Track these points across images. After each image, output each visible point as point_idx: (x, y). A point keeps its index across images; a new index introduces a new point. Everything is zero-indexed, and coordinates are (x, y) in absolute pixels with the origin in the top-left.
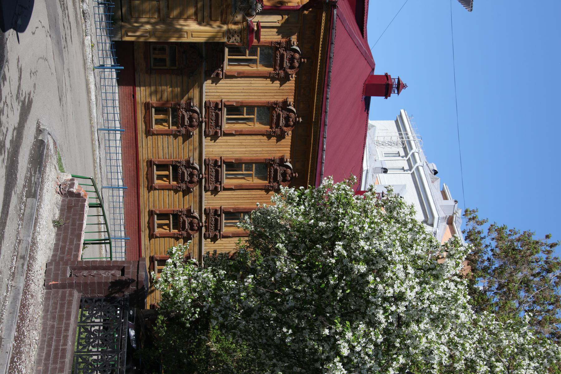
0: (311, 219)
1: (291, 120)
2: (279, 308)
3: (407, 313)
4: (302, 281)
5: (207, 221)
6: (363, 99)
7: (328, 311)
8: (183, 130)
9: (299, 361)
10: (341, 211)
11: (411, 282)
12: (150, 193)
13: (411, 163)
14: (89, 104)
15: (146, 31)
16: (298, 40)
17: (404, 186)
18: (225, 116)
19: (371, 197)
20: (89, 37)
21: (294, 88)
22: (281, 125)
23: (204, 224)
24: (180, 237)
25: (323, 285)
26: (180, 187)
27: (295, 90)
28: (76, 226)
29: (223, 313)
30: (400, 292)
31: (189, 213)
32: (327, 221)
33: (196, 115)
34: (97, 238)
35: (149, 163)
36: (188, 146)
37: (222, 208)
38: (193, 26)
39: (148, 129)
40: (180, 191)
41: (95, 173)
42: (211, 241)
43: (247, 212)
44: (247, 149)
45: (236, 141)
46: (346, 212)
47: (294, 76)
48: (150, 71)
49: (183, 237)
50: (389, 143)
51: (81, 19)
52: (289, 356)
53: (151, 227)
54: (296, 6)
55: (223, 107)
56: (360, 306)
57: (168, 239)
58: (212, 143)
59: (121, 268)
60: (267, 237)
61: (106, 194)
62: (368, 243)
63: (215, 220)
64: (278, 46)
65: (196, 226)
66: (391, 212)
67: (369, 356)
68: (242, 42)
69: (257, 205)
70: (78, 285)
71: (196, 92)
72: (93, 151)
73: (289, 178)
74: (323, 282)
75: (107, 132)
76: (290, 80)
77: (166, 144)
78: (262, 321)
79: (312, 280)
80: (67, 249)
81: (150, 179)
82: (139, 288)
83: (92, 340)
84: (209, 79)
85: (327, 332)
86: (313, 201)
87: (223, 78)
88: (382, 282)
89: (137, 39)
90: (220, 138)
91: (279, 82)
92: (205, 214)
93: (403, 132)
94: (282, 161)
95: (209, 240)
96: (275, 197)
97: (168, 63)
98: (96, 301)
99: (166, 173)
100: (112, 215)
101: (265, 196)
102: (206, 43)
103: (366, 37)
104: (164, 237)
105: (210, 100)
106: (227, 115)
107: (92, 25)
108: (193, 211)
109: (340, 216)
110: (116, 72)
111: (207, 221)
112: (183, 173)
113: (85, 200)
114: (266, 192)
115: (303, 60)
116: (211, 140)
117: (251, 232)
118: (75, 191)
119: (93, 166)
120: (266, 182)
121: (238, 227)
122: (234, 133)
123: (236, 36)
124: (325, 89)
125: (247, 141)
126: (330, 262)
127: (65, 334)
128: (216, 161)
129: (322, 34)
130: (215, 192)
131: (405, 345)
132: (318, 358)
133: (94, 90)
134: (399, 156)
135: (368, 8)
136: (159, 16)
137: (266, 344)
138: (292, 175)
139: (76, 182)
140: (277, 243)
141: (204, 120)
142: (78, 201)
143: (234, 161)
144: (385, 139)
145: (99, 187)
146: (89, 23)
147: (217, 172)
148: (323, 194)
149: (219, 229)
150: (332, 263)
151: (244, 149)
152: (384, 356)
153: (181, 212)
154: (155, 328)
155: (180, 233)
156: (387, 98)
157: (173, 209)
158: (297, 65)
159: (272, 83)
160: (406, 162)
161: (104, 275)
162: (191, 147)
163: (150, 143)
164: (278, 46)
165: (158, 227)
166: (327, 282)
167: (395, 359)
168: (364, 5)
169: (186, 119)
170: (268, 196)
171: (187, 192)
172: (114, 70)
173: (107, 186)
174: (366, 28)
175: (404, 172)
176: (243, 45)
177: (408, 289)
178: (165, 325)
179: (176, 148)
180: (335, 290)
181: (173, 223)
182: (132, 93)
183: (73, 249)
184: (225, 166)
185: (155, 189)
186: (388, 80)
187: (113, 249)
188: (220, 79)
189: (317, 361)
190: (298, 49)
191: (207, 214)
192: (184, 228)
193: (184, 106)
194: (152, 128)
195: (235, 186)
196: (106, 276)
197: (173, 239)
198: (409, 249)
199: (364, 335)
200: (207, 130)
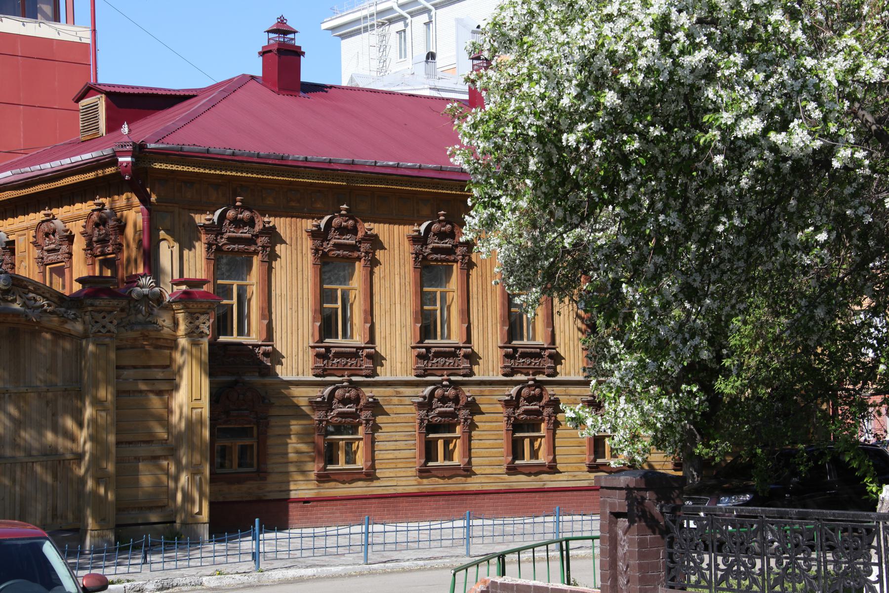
0: (526, 184)
1: (344, 224)
4: (635, 200)
6: (306, 95)
7: (687, 151)
9: (777, 202)
10: (509, 130)
11: (635, 7)
12: (477, 472)
13: (418, 10)
15: (192, 480)
16: (202, 212)
17: (459, 21)
18: (340, 341)
19: (485, 78)
20: (204, 579)
21: (288, 219)
23: (531, 377)
24: (553, 418)
25: (642, 160)
26: (466, 420)
27: (292, 217)
29: (687, 335)
30: (652, 26)
31: (512, 403)
32: (528, 154)
33: (338, 393)
34: (559, 564)
35: (424, 474)
36: (392, 407)
37: (502, 345)
38: (181, 399)
39: (363, 476)
40: (472, 420)
41: (442, 568)
42: (561, 364)
43: (509, 300)
44: (398, 301)
45: (383, 321)
46: (512, 121)
48: (261, 474)
49: (554, 413)
50: (382, 50)
52: (769, 220)
53: (536, 470)
54: (143, 215)
56: (679, 93)
57: (556, 440)
58: (387, 363)
59: (613, 518)
60: (552, 264)
61: (479, 549)
63: (523, 358)
65: (534, 390)
66: (511, 41)
67: (767, 77)
68: (209, 311)
69: (497, 283)
71: (296, 391)
72: (404, 571)
73: (448, 226)
74: (636, 160)
75: (370, 547)
76: (274, 225)
77: (391, 445)
78: (705, 267)
83: (742, 569)
84: (274, 369)
85: (719, 159)
86: (492, 181)
87: (272, 346)
88: (634, 57)
89: (206, 497)
90: (377, 349)
91: (279, 245)
92: (512, 376)
93: (362, 25)
94: (418, 240)
95: (559, 367)
96: (481, 253)
97: (247, 442)
98: (673, 562)
99: (440, 443)
100: (517, 538)
102: (211, 375)
103: (196, 90)
104: (554, 447)
106: (337, 337)
107: (183, 574)
109: (518, 132)
110: (266, 532)
112: (441, 414)
114: (472, 268)
115: (238, 204)
116: (382, 365)
117: (543, 292)
119: (430, 572)
121: (535, 317)
122: (368, 325)
123: (197, 323)
124: (290, 163)
125: (383, 302)
126: (601, 149)
128: (420, 356)
129: (191, 169)
130: (473, 358)
131: (750, 12)
132: (773, 166)
133: (297, 570)
134: (404, 31)
135: (142, 88)
136: (166, 458)
137: (746, 261)
138: (442, 221)
141: (346, 378)
143: (419, 325)
145: (467, 560)
147: (438, 355)
148: (480, 164)
149: (538, 350)
150: (604, 145)
153: (509, 417)
154: (718, 459)
156: (304, 53)
157: (504, 432)
158: (246, 214)
159: (280, 257)
160: (415, 19)
162: (395, 400)
163: (388, 473)
164: (214, 247)
165: (537, 458)
166: (636, 154)
167: (776, 30)
168: (139, 95)
169: (345, 409)
170: (479, 265)
171: (474, 408)
172: (261, 536)
173: (465, 547)
174: (178, 91)
175: (434, 22)
176: (214, 309)
177: (648, 11)
178: (712, 443)
179: (397, 427)
180: (650, 139)
181: (528, 432)
182: (301, 504)
184: (427, 341)
185: (469, 463)
186: (270, 51)
187: (575, 535)
189: (778, 169)
191: (513, 372)
192: (538, 413)
194: (362, 469)
195: (463, 323)
198: (576, 7)
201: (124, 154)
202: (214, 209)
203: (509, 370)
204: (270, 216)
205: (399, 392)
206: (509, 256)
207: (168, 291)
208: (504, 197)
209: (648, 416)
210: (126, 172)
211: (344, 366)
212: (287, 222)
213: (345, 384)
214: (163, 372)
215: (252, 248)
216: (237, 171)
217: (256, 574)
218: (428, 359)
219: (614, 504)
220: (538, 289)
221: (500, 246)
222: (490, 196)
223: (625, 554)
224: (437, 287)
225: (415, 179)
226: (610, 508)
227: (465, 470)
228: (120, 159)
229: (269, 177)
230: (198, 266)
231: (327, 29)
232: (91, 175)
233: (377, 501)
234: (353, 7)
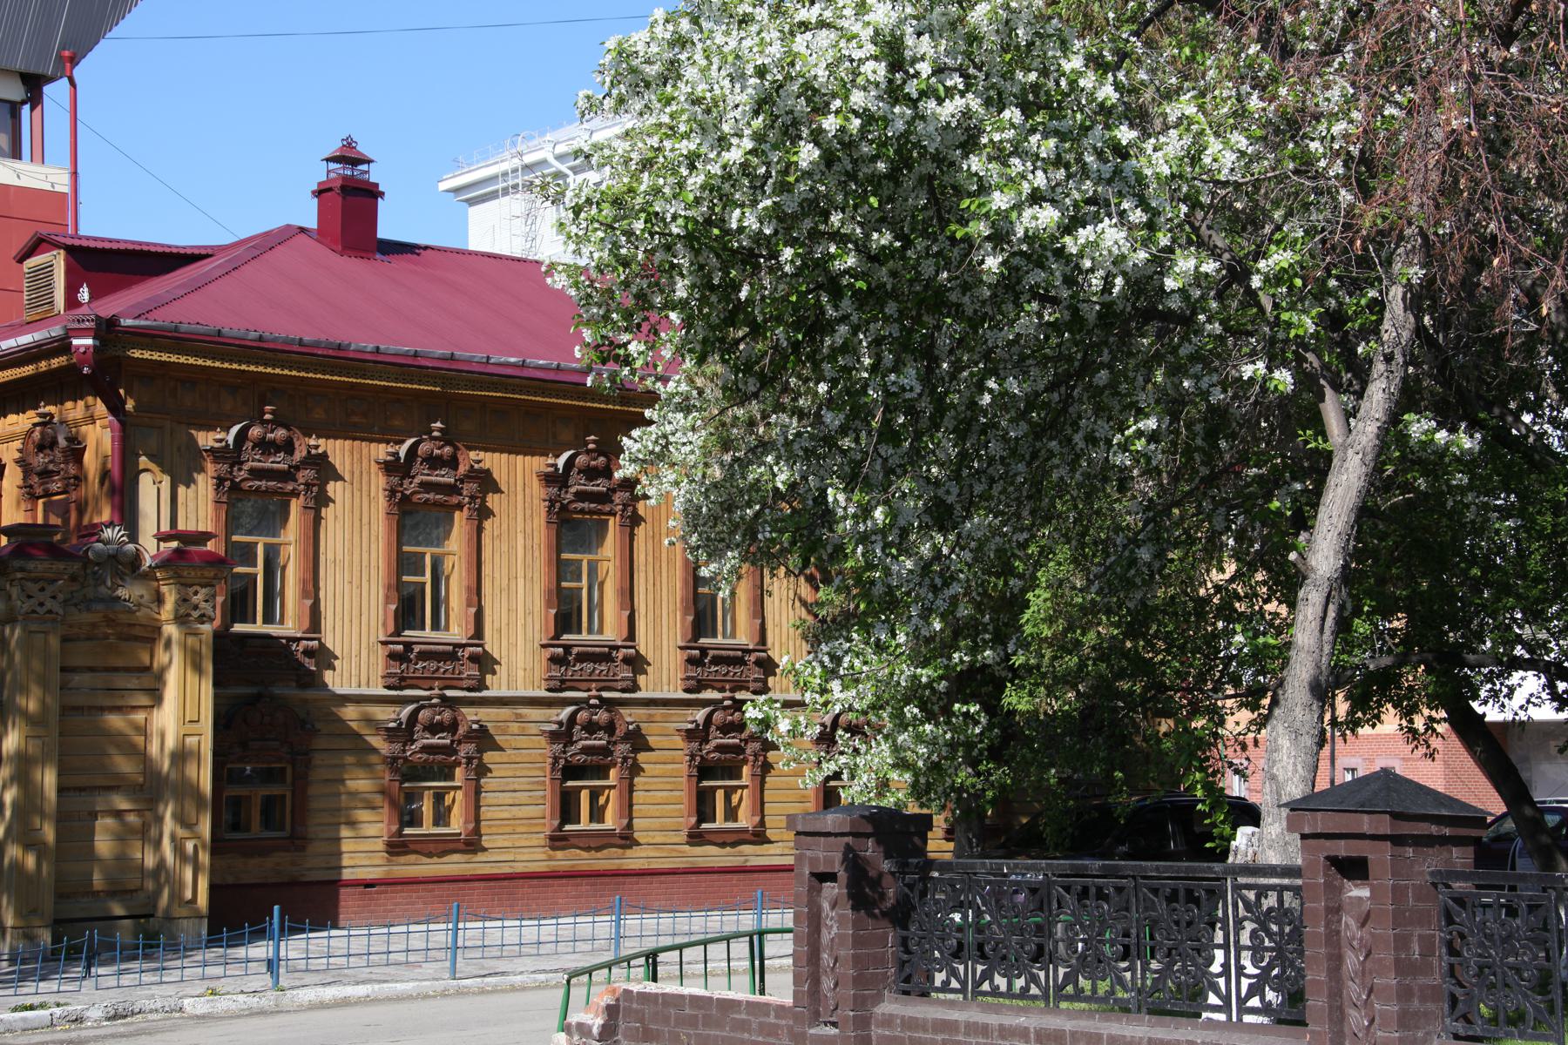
1: (437, 452)
2: (924, 423)
3: (936, 33)
5: (719, 685)
7: (932, 270)
8: (466, 749)
9: (1079, 374)
12: (641, 841)
14: (379, 1000)
16: (210, 427)
18: (428, 633)
20: (186, 1001)
21: (348, 443)
22: (452, 480)
23: (728, 694)
26: (625, 759)
27: (354, 439)
28: (696, 1016)
29: (938, 581)
31: (697, 735)
32: (674, 273)
33: (424, 715)
37: (683, 644)
40: (635, 759)
44: (520, 574)
45: (497, 605)
47: (312, 442)
48: (298, 841)
49: (762, 750)
50: (529, 222)
51: (132, 1023)
52: (1067, 401)
53: (734, 838)
55: (401, 639)
57: (766, 792)
58: (502, 670)
59: (815, 882)
60: (757, 515)
61: (630, 946)
62: (734, 141)
63: (716, 665)
64: (228, 484)
65: (732, 715)
69: (672, 544)
70: (860, 1003)
72: (513, 989)
73: (602, 459)
74: (851, 286)
76: (325, 452)
79: (844, 319)
80: (760, 1039)
81: (601, 841)
82: (869, 829)
84: (322, 676)
86: (614, 315)
87: (319, 639)
90: (488, 648)
91: (332, 483)
92: (699, 692)
93: (501, 185)
94: (552, 479)
95: (771, 679)
97: (275, 790)
98: (908, 951)
99: (585, 796)
101: (649, 526)
104: (762, 803)
105: (380, 674)
108: (692, 722)
111: (719, 685)
112: (586, 750)
113: (627, 992)
115: (268, 417)
116: (494, 673)
117: (744, 559)
118: (599, 1021)
120: (611, 523)
122: (473, 610)
124: (351, 356)
125: (497, 575)
126: (792, 261)
127: (996, 1034)
128: (553, 660)
129: (192, 361)
130: (637, 663)
135: (126, 242)
139: (574, 1018)
140: (776, 489)
141: (437, 691)
142: (628, 1011)
143: (553, 611)
144: (518, 232)
146: (148, 1004)
147: (582, 658)
149: (740, 653)
150: (797, 255)
151: (521, 581)
152: (1065, 117)
153: (693, 757)
155: (751, 758)
157: (684, 780)
158: (281, 433)
159: (334, 502)
161: (835, 930)
162: (515, 727)
163: (500, 841)
164: (228, 484)
165: (736, 820)
167: (1073, 83)
169: (435, 741)
170: (649, 520)
171: (637, 740)
174: (184, 248)
177: (866, 18)
179: (516, 769)
181: (723, 779)
182: (361, 889)
183: (761, 1019)
184: (565, 637)
185: (630, 826)
186: (330, 189)
188: (322, 645)
190: (235, 429)
191: (701, 686)
192: (738, 750)
193: (398, 747)
196: (836, 922)
197: (767, 779)
199: (1003, 164)
200: (465, 684)
201: (81, 333)
202: (228, 424)
203: (693, 682)
204: (318, 437)
205: (520, 715)
206: (691, 501)
207: (150, 547)
208: (634, 343)
209: (905, 751)
210: (83, 363)
211: (434, 672)
212: (347, 448)
213: (435, 701)
214: (138, 678)
215: (290, 487)
216: (266, 365)
217: (272, 995)
218: (568, 664)
219: (817, 859)
220: (736, 554)
221: (677, 483)
222: (611, 343)
223: (832, 940)
224: (584, 553)
225: (549, 385)
226: (811, 865)
227: (622, 837)
228: (76, 342)
229: (318, 376)
230: (202, 514)
231: (448, 191)
232: (28, 370)
233: (482, 884)
234: (487, 158)
